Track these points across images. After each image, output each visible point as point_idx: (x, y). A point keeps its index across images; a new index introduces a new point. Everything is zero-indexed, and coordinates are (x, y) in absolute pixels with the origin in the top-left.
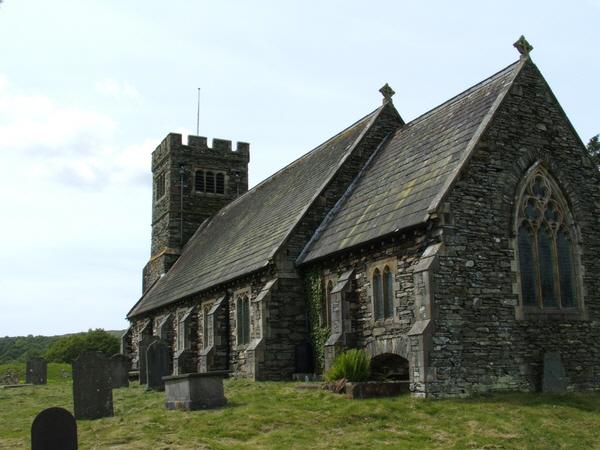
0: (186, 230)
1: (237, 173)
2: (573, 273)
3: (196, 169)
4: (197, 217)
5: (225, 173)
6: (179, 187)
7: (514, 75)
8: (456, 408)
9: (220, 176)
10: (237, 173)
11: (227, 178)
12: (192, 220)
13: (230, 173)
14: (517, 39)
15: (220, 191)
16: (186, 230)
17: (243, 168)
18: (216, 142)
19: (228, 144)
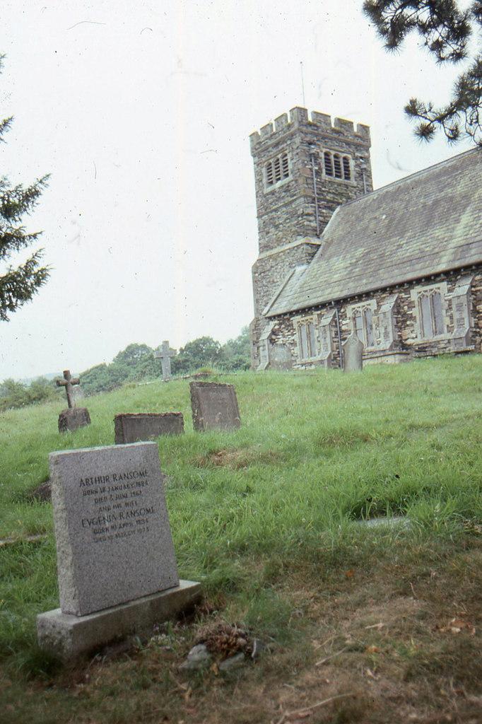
0: (321, 218)
1: (361, 158)
2: (341, 489)
3: (324, 150)
4: (330, 204)
5: (349, 156)
6: (311, 169)
7: (188, 598)
8: (244, 717)
9: (346, 160)
10: (361, 158)
11: (352, 163)
12: (326, 207)
13: (356, 158)
14: (407, 103)
15: (348, 178)
16: (321, 218)
17: (366, 154)
18: (316, 114)
19: (349, 124)
